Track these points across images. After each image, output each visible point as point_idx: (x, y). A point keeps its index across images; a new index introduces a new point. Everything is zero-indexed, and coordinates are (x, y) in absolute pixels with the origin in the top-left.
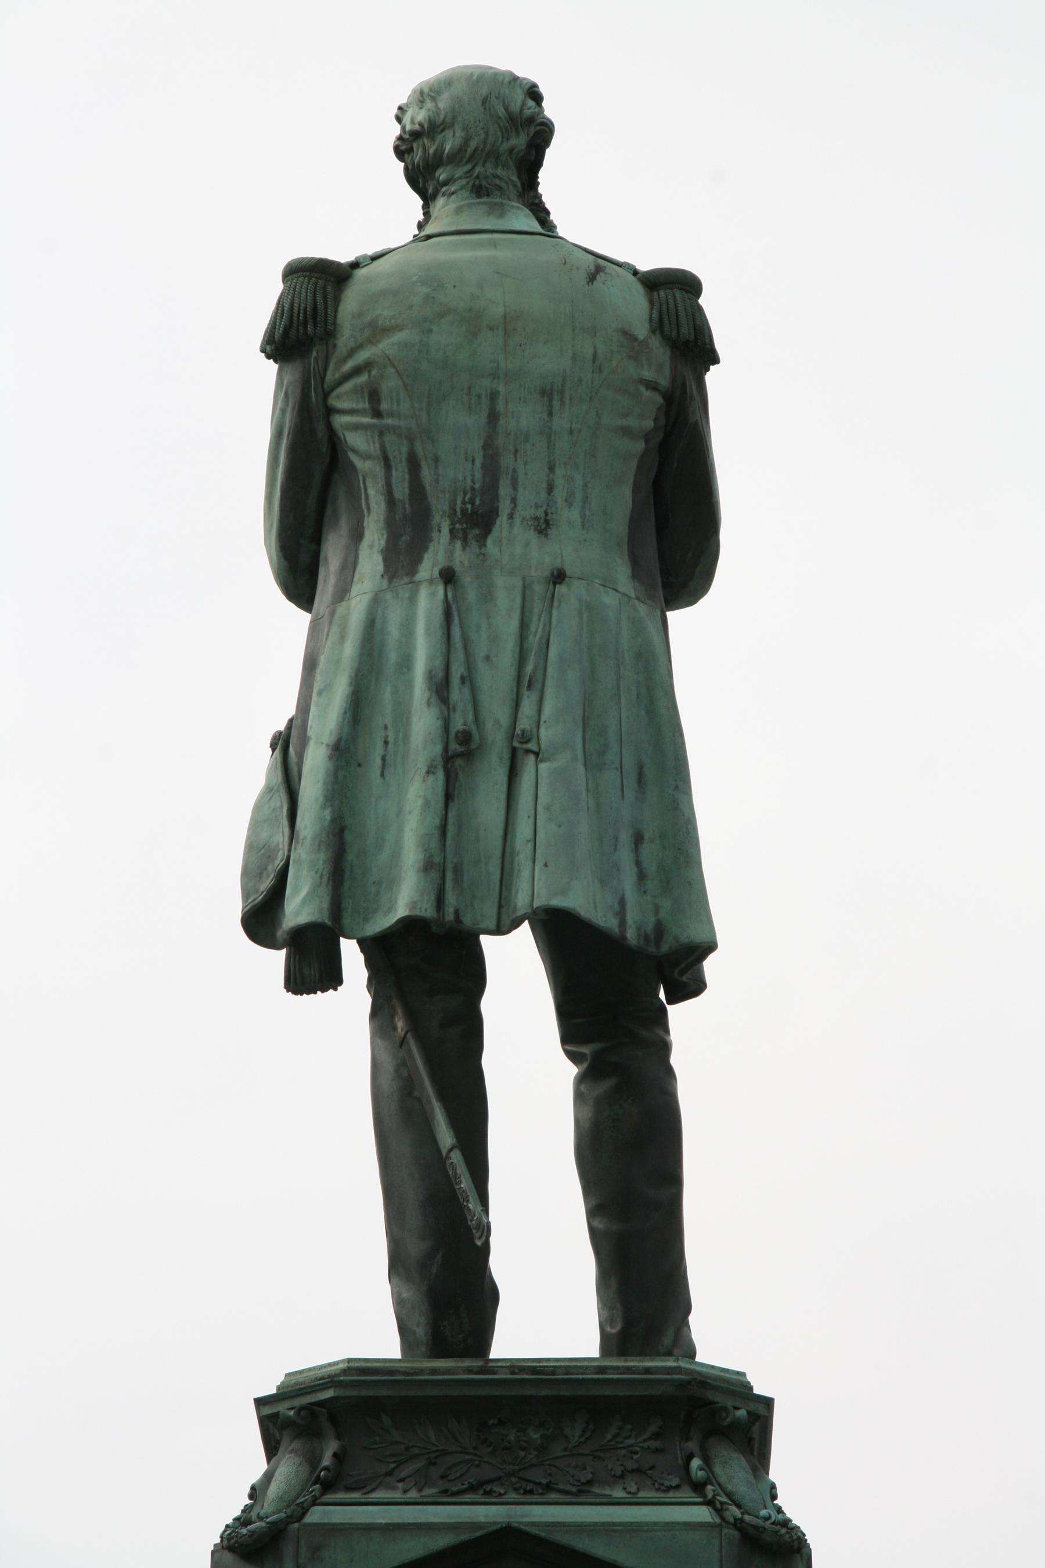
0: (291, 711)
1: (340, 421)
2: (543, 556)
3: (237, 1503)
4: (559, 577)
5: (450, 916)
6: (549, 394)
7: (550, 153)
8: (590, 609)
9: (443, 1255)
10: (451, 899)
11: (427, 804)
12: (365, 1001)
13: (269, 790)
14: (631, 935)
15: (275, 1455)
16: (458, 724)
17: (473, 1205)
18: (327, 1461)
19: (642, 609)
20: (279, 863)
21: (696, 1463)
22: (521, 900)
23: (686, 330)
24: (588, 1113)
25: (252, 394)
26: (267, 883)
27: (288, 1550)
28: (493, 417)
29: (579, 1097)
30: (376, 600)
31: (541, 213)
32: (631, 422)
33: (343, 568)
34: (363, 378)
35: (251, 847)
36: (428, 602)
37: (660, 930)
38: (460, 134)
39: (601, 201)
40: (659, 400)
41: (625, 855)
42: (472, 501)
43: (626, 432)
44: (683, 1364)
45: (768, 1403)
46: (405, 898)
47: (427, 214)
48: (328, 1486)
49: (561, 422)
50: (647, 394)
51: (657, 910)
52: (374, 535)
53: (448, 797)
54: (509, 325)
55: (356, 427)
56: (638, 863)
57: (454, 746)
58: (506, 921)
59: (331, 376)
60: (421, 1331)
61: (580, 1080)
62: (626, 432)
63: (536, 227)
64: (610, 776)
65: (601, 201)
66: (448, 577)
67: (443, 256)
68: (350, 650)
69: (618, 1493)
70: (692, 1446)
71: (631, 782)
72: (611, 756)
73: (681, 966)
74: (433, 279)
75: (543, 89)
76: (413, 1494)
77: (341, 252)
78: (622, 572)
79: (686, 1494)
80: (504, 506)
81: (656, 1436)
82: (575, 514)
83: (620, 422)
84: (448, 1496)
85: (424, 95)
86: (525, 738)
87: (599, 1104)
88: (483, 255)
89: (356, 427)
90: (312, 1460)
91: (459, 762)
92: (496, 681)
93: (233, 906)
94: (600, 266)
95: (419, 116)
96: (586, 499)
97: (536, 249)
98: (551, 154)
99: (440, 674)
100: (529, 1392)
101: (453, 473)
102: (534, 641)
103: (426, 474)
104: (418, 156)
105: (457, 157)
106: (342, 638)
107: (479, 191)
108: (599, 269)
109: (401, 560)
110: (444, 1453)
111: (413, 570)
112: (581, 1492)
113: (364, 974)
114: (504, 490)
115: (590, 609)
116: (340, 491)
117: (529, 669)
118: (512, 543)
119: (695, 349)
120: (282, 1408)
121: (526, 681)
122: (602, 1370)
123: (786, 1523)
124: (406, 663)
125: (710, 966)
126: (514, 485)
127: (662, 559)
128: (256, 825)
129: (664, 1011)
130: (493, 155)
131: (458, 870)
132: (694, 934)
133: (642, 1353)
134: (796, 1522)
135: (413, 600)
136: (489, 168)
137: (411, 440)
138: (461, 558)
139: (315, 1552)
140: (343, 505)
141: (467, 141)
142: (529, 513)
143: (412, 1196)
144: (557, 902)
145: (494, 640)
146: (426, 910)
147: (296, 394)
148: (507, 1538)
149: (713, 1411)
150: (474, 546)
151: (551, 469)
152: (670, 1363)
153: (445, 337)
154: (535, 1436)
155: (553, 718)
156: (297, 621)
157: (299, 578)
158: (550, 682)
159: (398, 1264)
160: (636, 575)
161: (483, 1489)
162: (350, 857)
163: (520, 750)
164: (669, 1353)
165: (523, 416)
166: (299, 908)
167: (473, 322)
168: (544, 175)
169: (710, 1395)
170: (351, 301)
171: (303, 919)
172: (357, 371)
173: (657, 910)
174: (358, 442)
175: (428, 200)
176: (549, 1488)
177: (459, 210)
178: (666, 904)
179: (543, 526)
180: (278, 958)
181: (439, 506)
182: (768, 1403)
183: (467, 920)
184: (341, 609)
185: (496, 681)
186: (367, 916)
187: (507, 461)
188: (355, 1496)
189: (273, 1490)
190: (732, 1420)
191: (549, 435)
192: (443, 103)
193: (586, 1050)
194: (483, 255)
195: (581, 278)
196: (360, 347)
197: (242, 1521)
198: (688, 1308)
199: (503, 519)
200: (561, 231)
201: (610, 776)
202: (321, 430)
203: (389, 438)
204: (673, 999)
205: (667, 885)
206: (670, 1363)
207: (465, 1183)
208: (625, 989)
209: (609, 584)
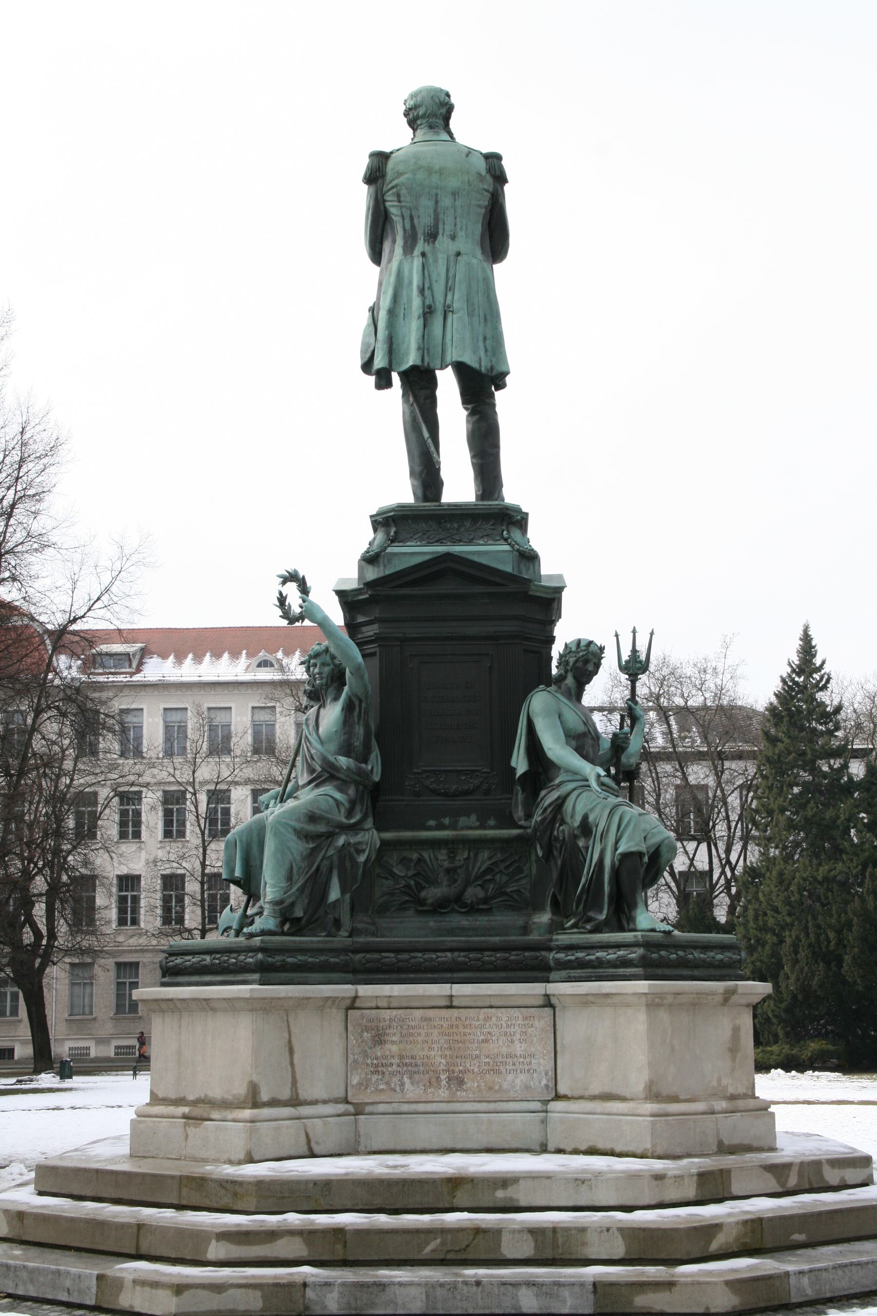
0: (374, 299)
1: (388, 204)
2: (453, 247)
3: (365, 547)
4: (458, 254)
5: (426, 364)
6: (455, 194)
7: (453, 114)
8: (469, 264)
9: (427, 474)
10: (426, 359)
11: (418, 329)
12: (401, 392)
13: (368, 325)
14: (483, 369)
15: (299, 838)
16: (427, 302)
17: (435, 455)
18: (392, 534)
19: (485, 264)
20: (372, 348)
21: (505, 533)
22: (448, 359)
23: (498, 173)
24: (470, 426)
25: (360, 197)
26: (369, 355)
27: (381, 560)
28: (437, 202)
29: (468, 421)
30: (401, 263)
31: (450, 134)
32: (481, 203)
33: (390, 252)
34: (395, 190)
35: (363, 343)
36: (417, 262)
37: (492, 368)
38: (424, 108)
39: (470, 131)
40: (489, 195)
41: (481, 344)
42: (833, 959)
43: (479, 206)
44: (501, 503)
45: (527, 514)
46: (412, 359)
47: (414, 136)
48: (393, 541)
49: (458, 203)
50: (486, 193)
51: (491, 361)
52: (400, 241)
53: (425, 326)
54: (441, 172)
55: (393, 206)
56: (485, 347)
57: (426, 310)
58: (444, 365)
59: (385, 189)
60: (420, 494)
61: (468, 416)
62: (479, 206)
63: (449, 138)
64: (476, 319)
65: (470, 131)
66: (423, 255)
67: (420, 149)
68: (393, 279)
69: (481, 542)
70: (504, 527)
71: (482, 320)
72: (476, 312)
73: (499, 380)
74: (417, 157)
75: (450, 93)
76: (419, 543)
77: (387, 149)
78: (479, 252)
79: (502, 542)
80: (441, 231)
81: (493, 525)
82: (463, 233)
83: (477, 203)
84: (430, 544)
85: (413, 96)
86: (449, 307)
87: (474, 423)
88: (433, 149)
89: (393, 206)
90: (388, 534)
91: (428, 315)
92: (439, 288)
93: (358, 363)
94: (470, 152)
95: (411, 103)
96: (467, 229)
97: (449, 146)
98: (453, 115)
99: (421, 287)
100: (453, 512)
101: (424, 221)
102: (451, 275)
103: (416, 221)
104: (411, 116)
105: (423, 116)
106: (390, 275)
107: (431, 127)
108: (469, 152)
109: (408, 249)
110: (428, 531)
111: (412, 253)
112: (470, 542)
113: (400, 383)
114: (441, 226)
115: (469, 264)
116: (388, 227)
117: (449, 284)
118: (443, 242)
119: (500, 178)
120: (378, 518)
121: (449, 288)
122: (476, 505)
123: (532, 550)
124: (410, 283)
125: (508, 379)
126: (444, 224)
127: (491, 247)
128: (364, 336)
129: (493, 394)
130: (435, 115)
131: (428, 350)
132: (503, 369)
133: (488, 500)
134: (535, 549)
135: (412, 262)
136: (434, 120)
137: (411, 210)
138: (427, 248)
139: (389, 561)
140: (389, 231)
141: (426, 111)
142: (448, 233)
143: (416, 452)
144: (460, 359)
145: (438, 275)
146: (419, 363)
147: (374, 195)
148: (448, 555)
149: (510, 517)
150: (431, 244)
151: (455, 218)
152: (497, 503)
153: (421, 176)
154: (456, 525)
155: (458, 300)
156: (376, 269)
157: (376, 255)
158: (456, 289)
159: (412, 474)
160: (483, 253)
161: (440, 542)
162: (394, 346)
163: (447, 311)
164: (496, 500)
165: (446, 201)
166: (379, 362)
167: (430, 171)
168: (452, 122)
169: (510, 512)
170: (390, 164)
171: (380, 366)
172: (393, 188)
173: (491, 361)
174: (394, 211)
175: (414, 130)
176: (460, 541)
177: (425, 134)
178: (494, 360)
179: (453, 237)
180: (372, 379)
181: (420, 231)
182: (527, 514)
183: (432, 366)
184: (389, 266)
185: (439, 288)
186: (400, 365)
187: (441, 216)
188: (401, 544)
189: (376, 543)
190: (515, 520)
191: (454, 207)
192: (419, 99)
193: (470, 406)
194: (433, 149)
195: (464, 155)
196: (394, 180)
197: (367, 552)
198: (502, 486)
199: (440, 236)
200: (457, 140)
201: (476, 319)
202: (382, 208)
203: (404, 210)
204: (496, 390)
205: (494, 354)
206: (497, 503)
207: (432, 449)
208: (481, 387)
209: (474, 256)
